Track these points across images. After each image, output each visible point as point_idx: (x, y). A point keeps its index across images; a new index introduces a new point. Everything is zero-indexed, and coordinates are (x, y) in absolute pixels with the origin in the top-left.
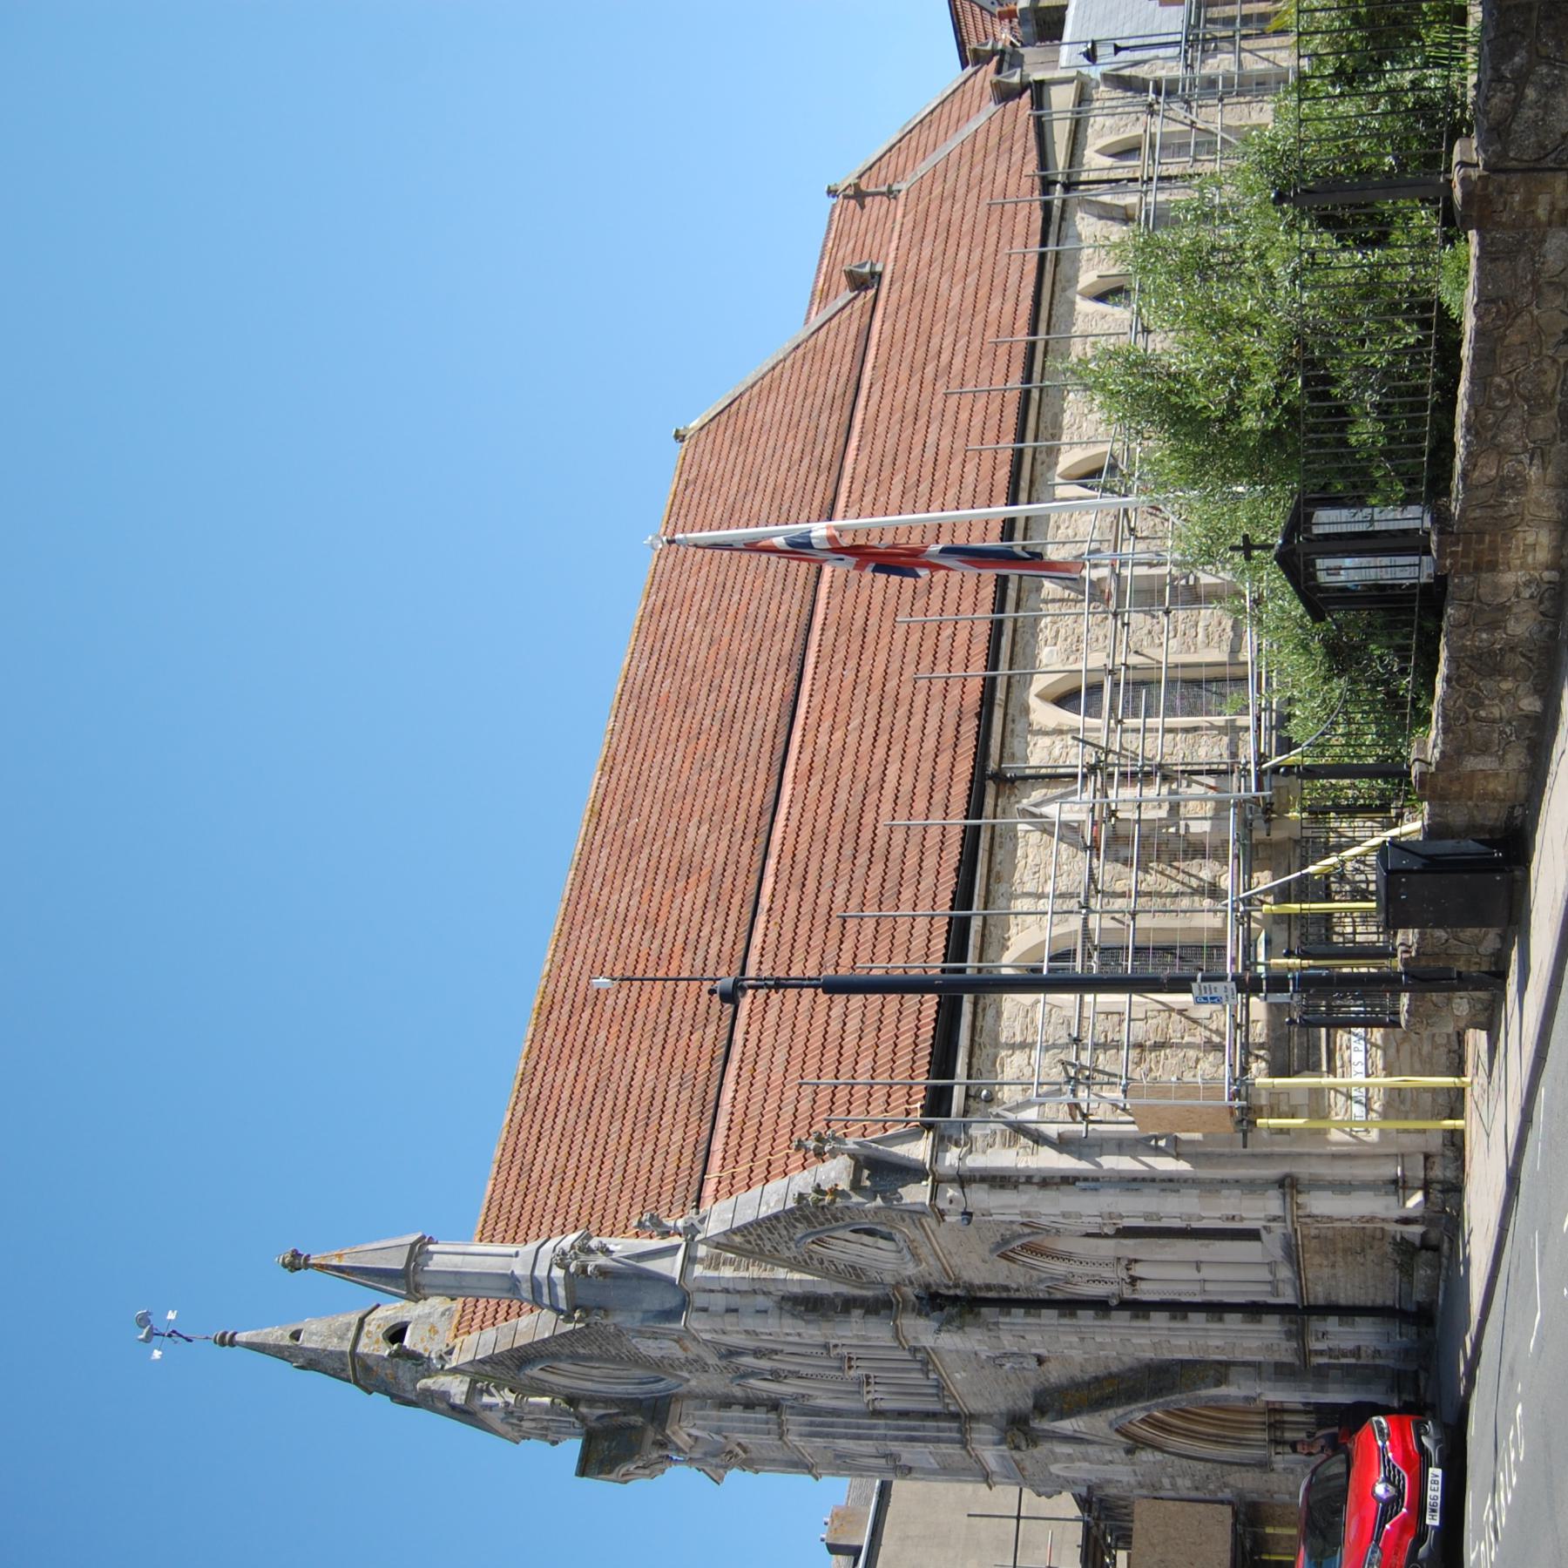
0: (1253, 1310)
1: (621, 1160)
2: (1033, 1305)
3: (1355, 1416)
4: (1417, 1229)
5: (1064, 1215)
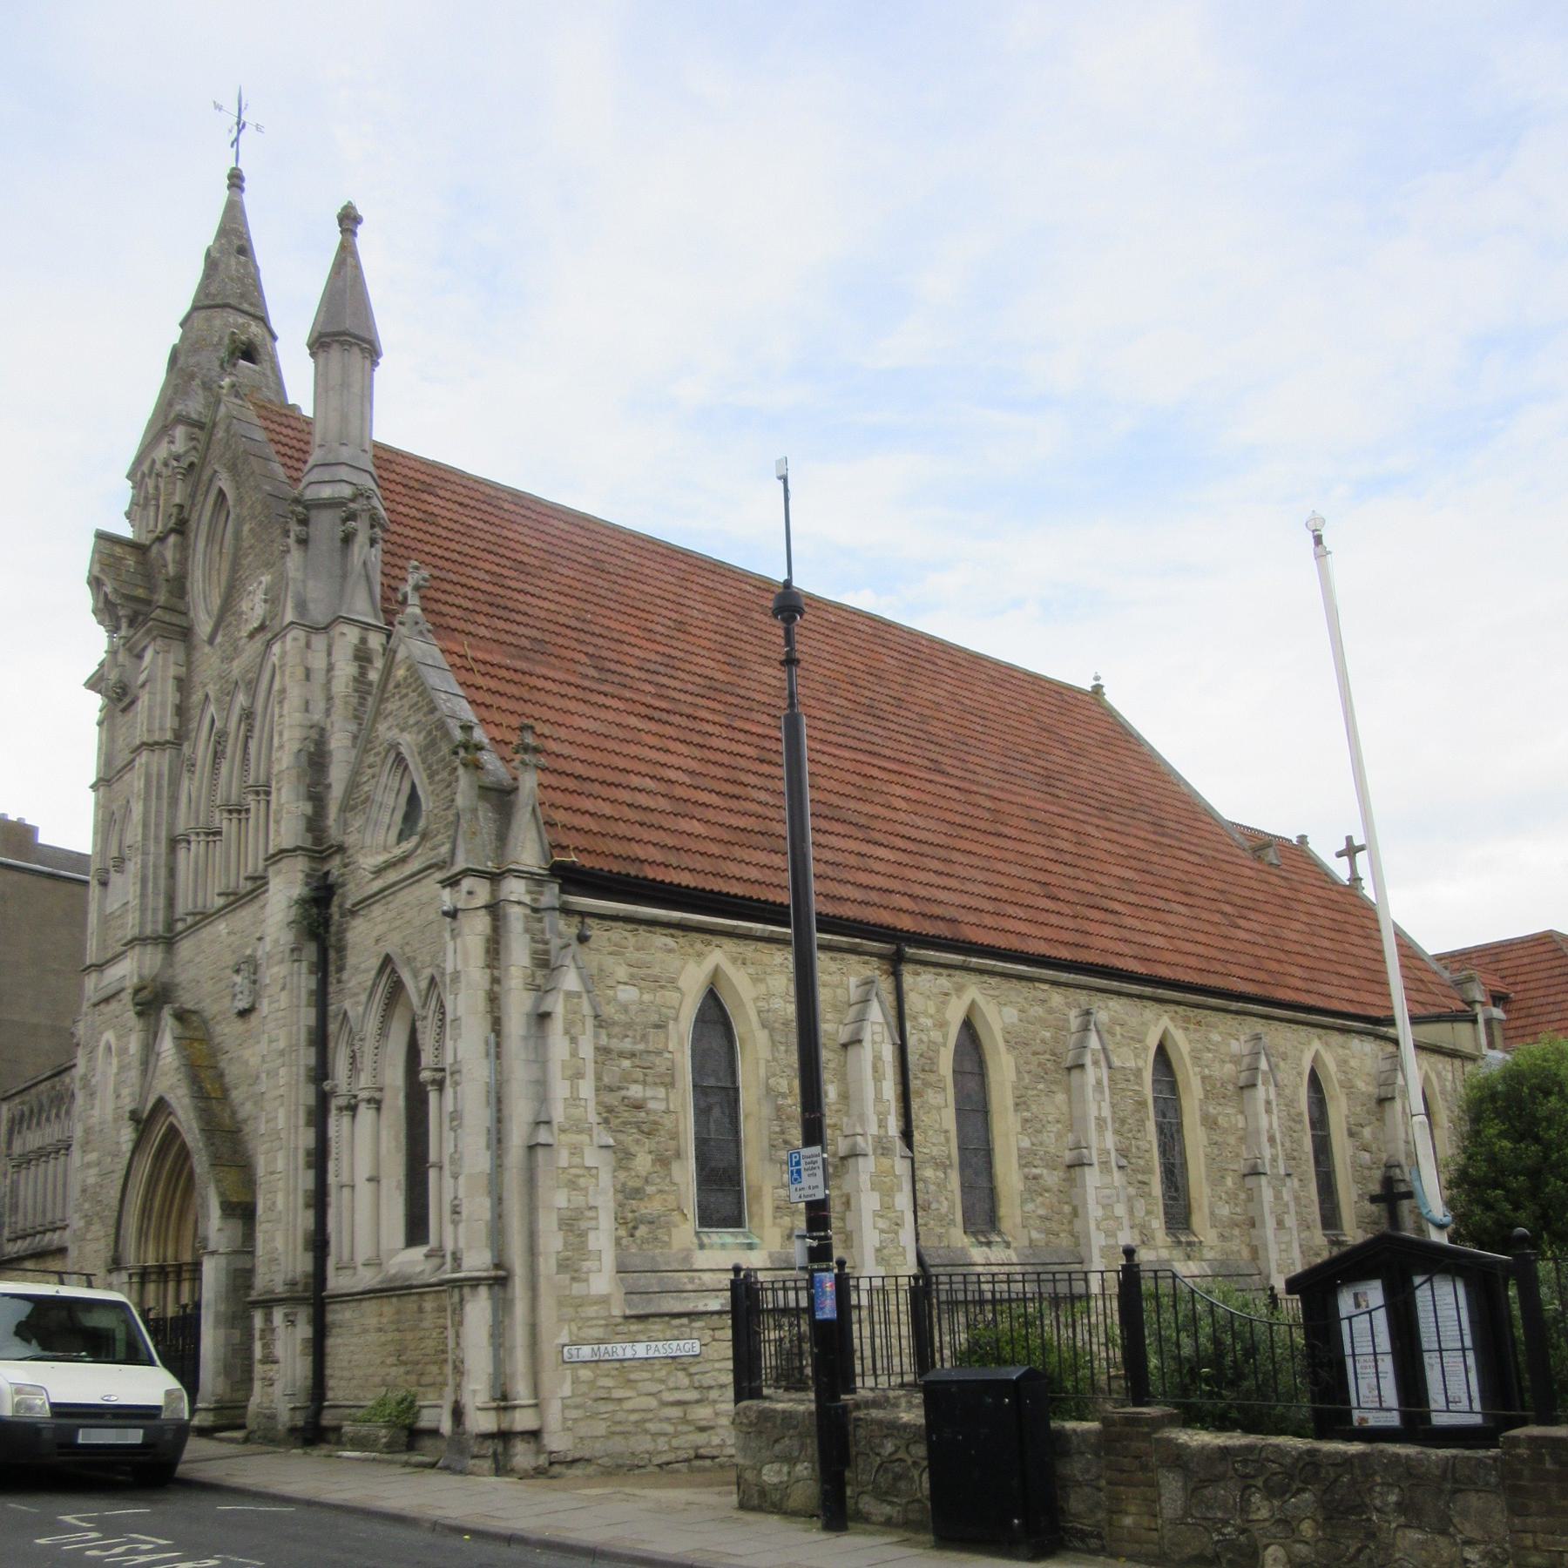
0: (319, 1243)
2: (321, 998)
3: (184, 1365)
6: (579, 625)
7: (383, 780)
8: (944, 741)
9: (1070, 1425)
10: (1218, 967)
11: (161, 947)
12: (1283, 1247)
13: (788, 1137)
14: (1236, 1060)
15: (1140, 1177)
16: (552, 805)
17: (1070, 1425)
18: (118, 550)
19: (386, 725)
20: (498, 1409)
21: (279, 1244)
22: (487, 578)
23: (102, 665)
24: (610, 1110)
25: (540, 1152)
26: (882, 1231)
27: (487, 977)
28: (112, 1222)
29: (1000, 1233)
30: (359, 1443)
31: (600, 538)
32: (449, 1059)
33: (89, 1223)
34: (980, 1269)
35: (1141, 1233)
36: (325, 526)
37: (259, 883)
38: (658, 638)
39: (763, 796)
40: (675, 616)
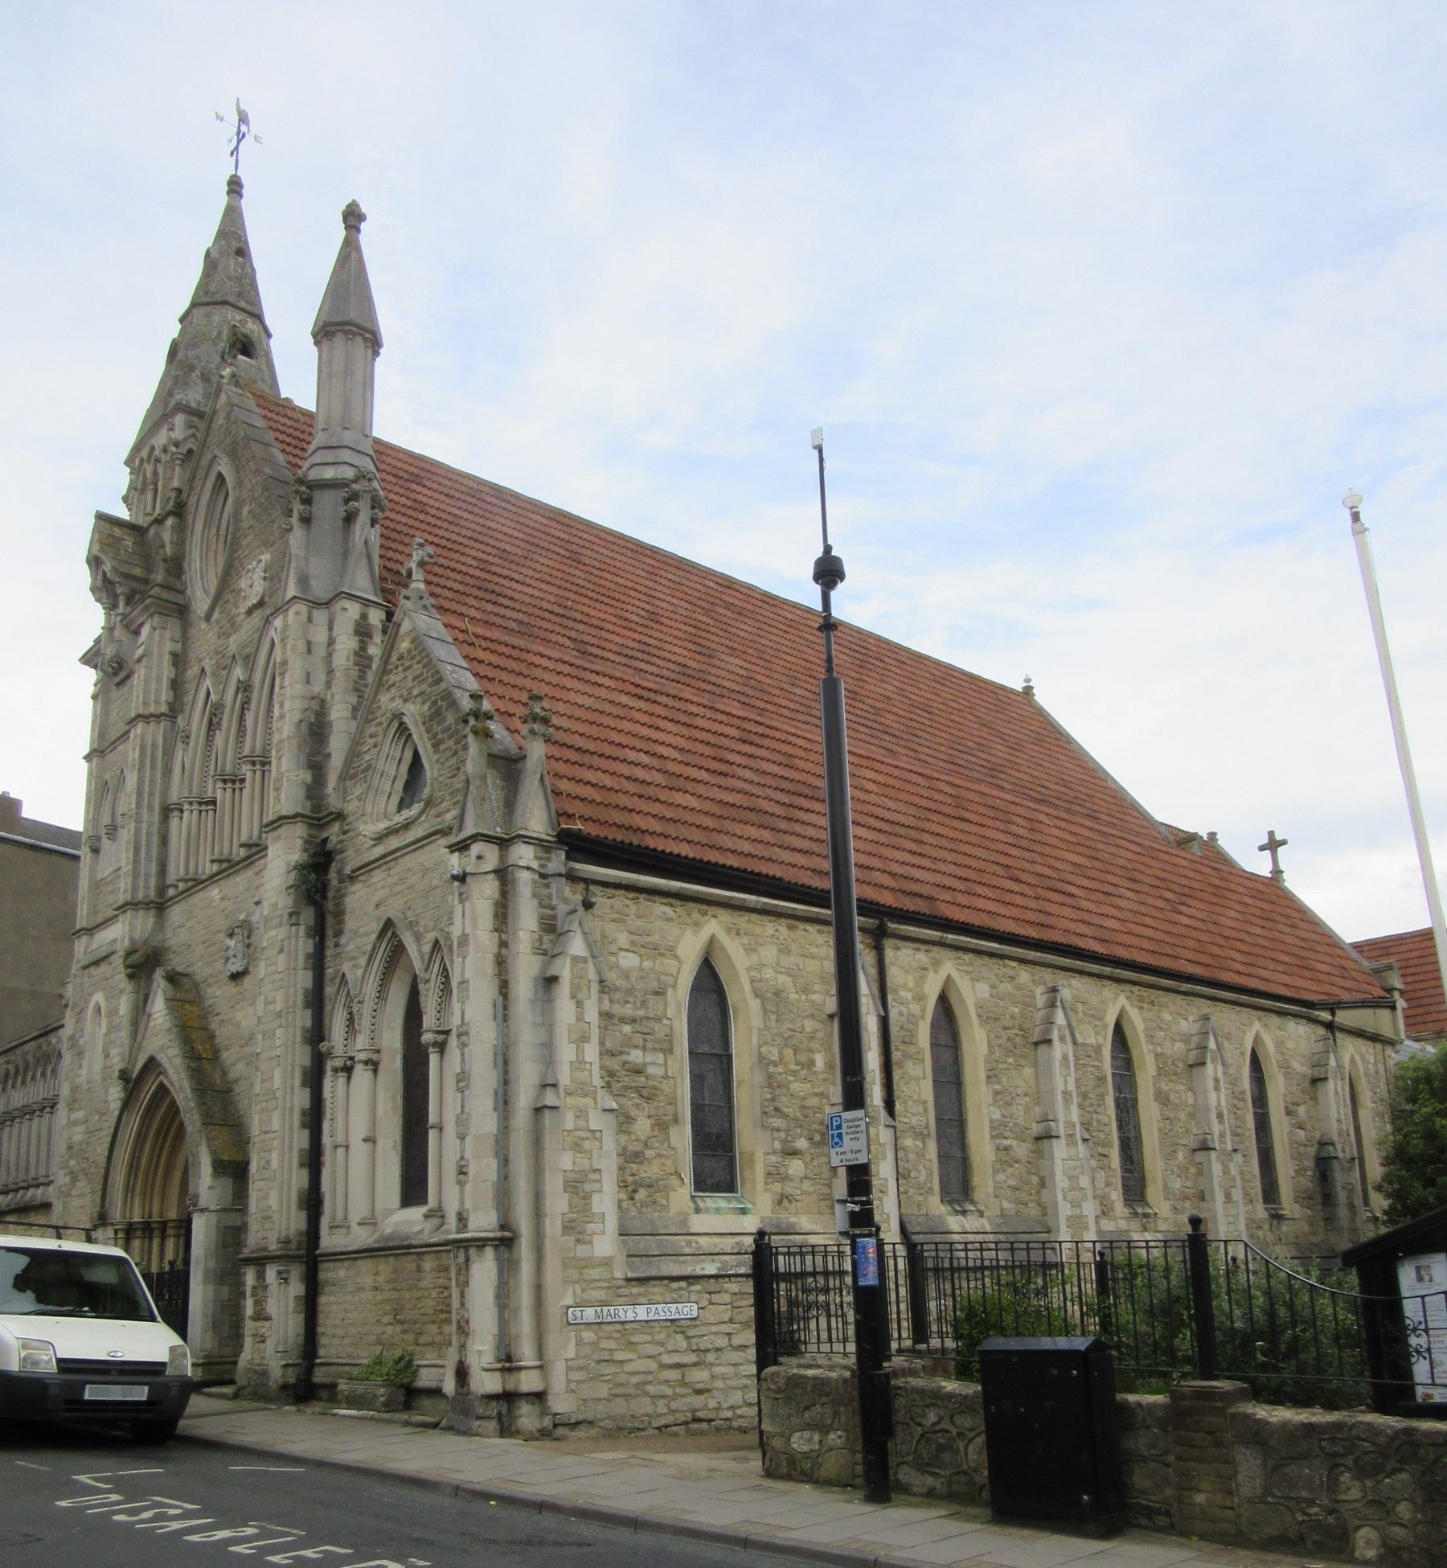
0: (312, 1202)
2: (318, 962)
6: (561, 611)
7: (386, 749)
8: (897, 733)
9: (1132, 1398)
10: (1167, 949)
11: (152, 912)
12: (1231, 1219)
13: (778, 1104)
14: (1186, 1039)
15: (1100, 1150)
16: (556, 775)
17: (1132, 1398)
18: (117, 532)
19: (388, 696)
20: (502, 1370)
21: (273, 1202)
22: (475, 563)
23: (98, 641)
27: (496, 940)
28: (100, 1179)
29: (973, 1202)
30: (355, 1401)
31: (574, 531)
32: (456, 1021)
33: (74, 1180)
34: (956, 1237)
35: (1101, 1204)
36: (328, 505)
37: (256, 850)
38: (634, 626)
39: (748, 774)
40: (647, 607)
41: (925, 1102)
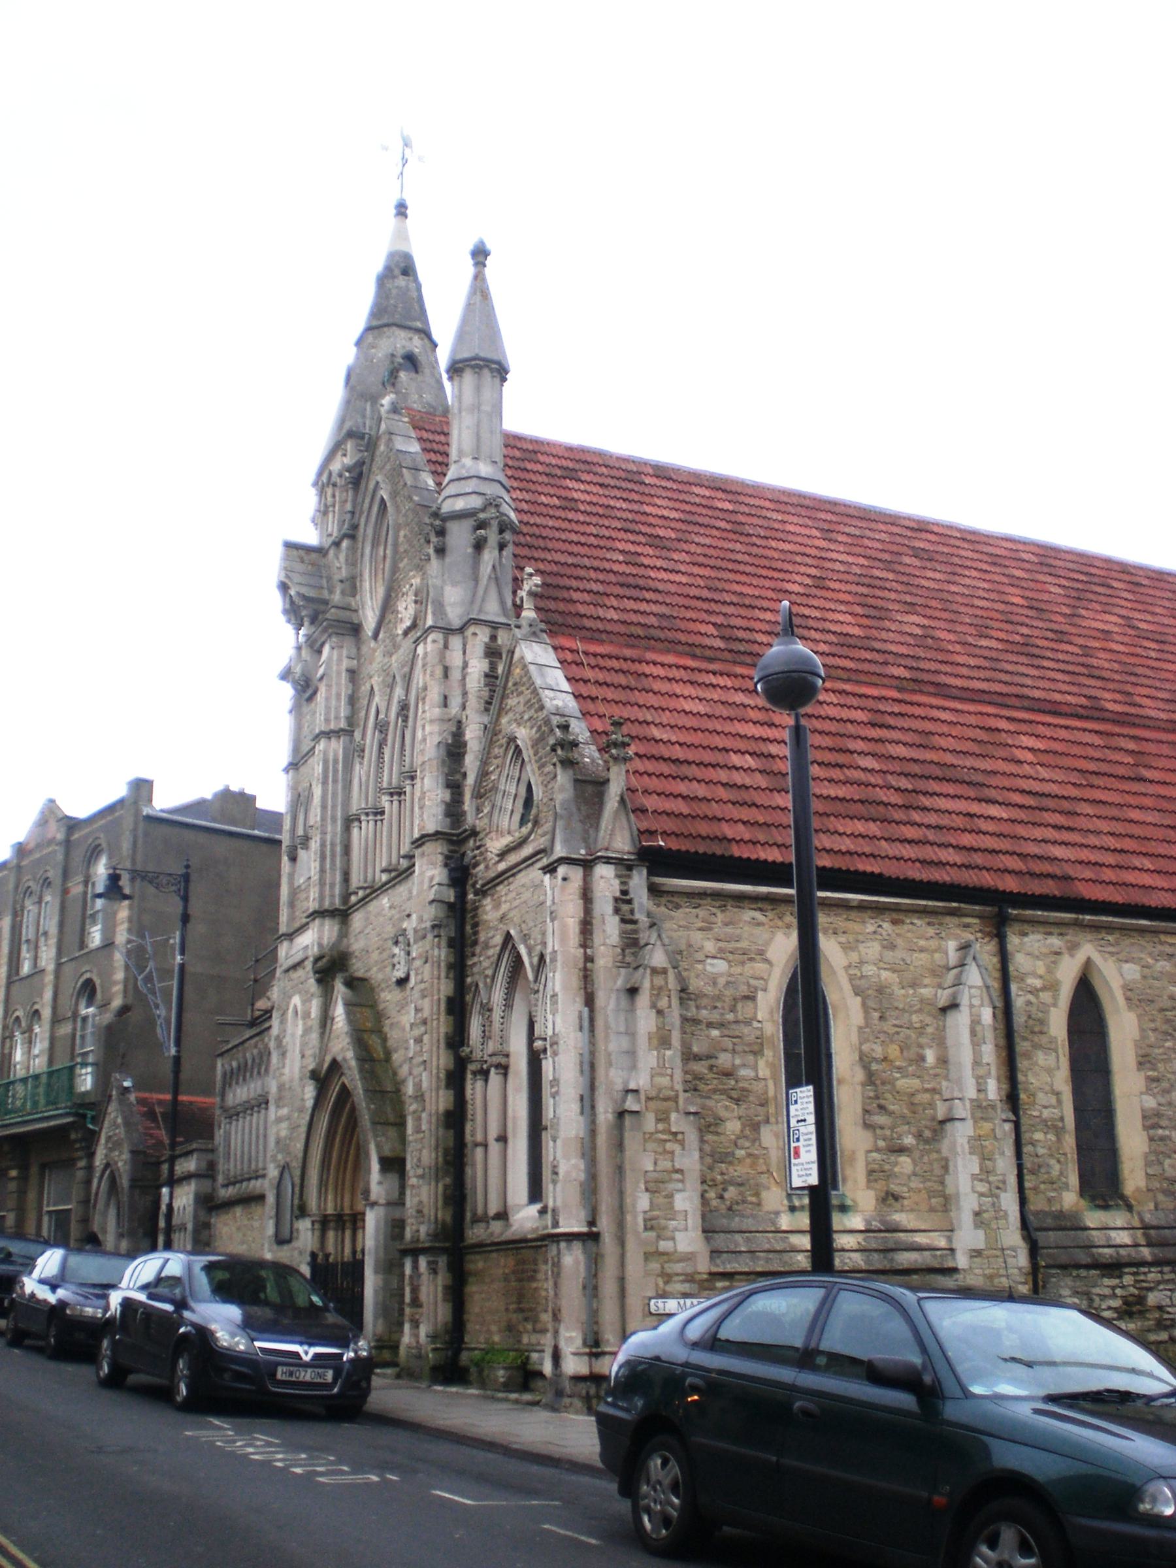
1: (586, 562)
4: (547, 1368)
5: (554, 995)
13: (882, 1102)
16: (645, 792)
24: (698, 1077)
25: (628, 1120)
26: (982, 1195)
36: (460, 536)
41: (1058, 1094)
